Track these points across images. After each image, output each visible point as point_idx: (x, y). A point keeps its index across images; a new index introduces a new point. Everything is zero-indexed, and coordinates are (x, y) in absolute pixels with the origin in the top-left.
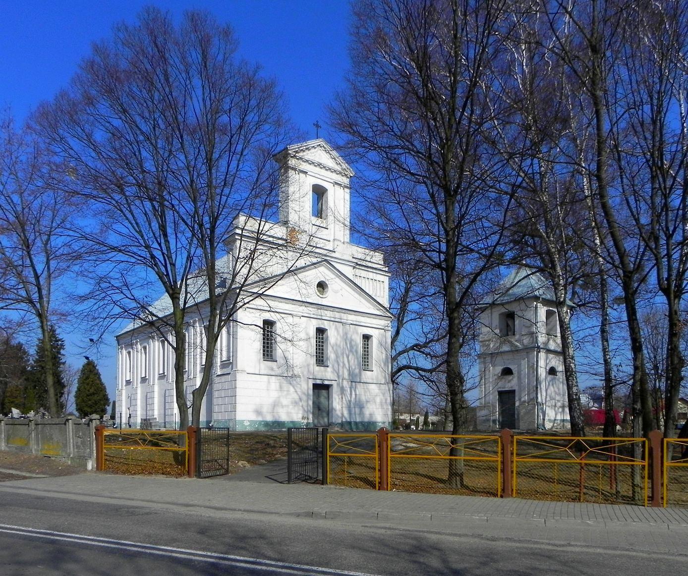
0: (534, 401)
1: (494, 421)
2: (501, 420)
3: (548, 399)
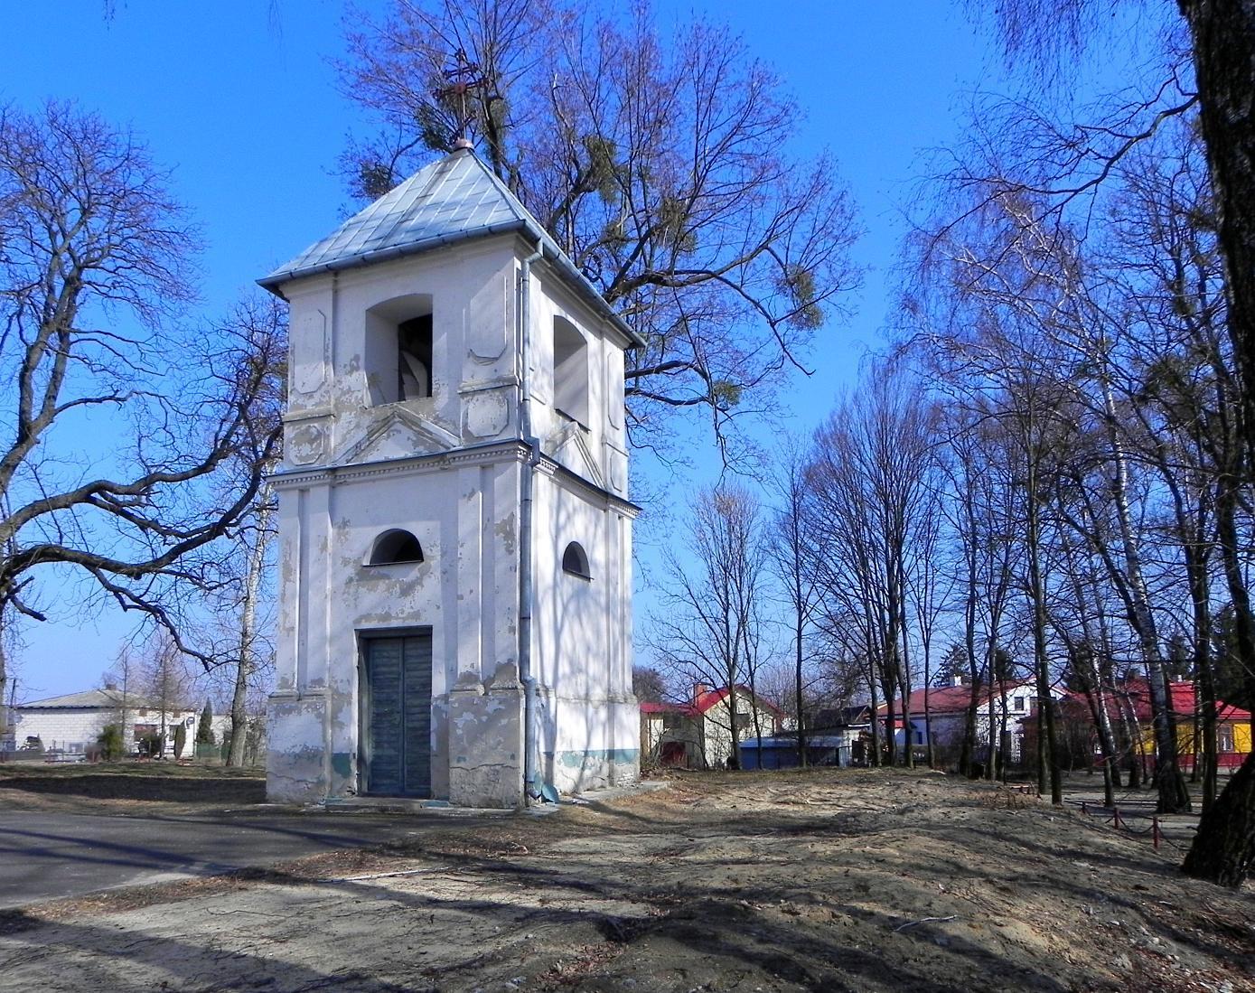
0: (512, 682)
1: (340, 762)
2: (368, 752)
3: (564, 668)
